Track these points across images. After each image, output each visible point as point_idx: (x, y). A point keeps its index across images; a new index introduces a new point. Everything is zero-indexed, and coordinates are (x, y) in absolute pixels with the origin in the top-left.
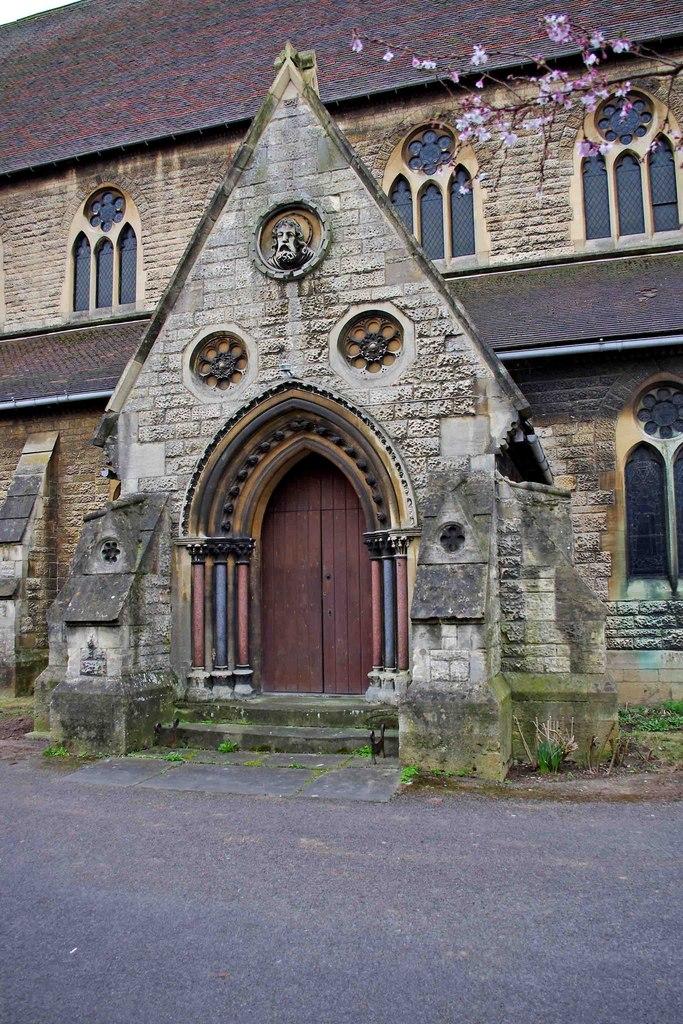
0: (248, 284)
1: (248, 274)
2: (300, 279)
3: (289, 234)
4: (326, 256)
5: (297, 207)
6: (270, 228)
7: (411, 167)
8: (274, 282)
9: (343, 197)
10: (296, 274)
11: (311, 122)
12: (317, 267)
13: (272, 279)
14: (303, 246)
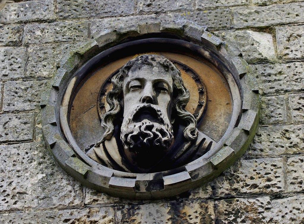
0: (30, 200)
1: (31, 180)
2: (178, 197)
3: (158, 86)
4: (247, 148)
5: (172, 43)
6: (93, 85)
7: (157, 131)
8: (103, 199)
9: (282, 33)
10: (168, 180)
11: (255, 38)
12: (222, 171)
13: (98, 190)
14: (186, 122)
